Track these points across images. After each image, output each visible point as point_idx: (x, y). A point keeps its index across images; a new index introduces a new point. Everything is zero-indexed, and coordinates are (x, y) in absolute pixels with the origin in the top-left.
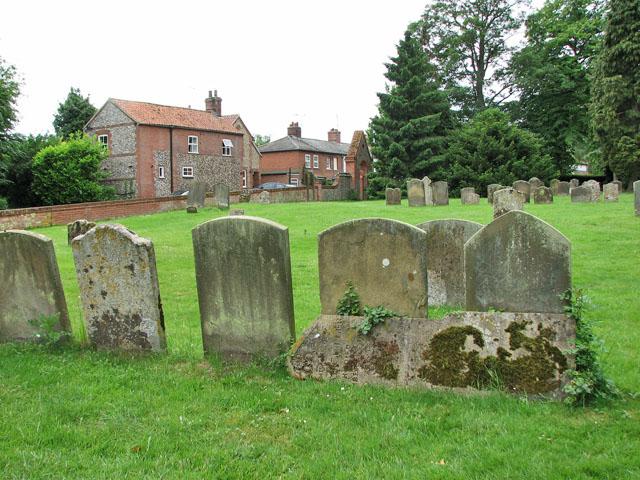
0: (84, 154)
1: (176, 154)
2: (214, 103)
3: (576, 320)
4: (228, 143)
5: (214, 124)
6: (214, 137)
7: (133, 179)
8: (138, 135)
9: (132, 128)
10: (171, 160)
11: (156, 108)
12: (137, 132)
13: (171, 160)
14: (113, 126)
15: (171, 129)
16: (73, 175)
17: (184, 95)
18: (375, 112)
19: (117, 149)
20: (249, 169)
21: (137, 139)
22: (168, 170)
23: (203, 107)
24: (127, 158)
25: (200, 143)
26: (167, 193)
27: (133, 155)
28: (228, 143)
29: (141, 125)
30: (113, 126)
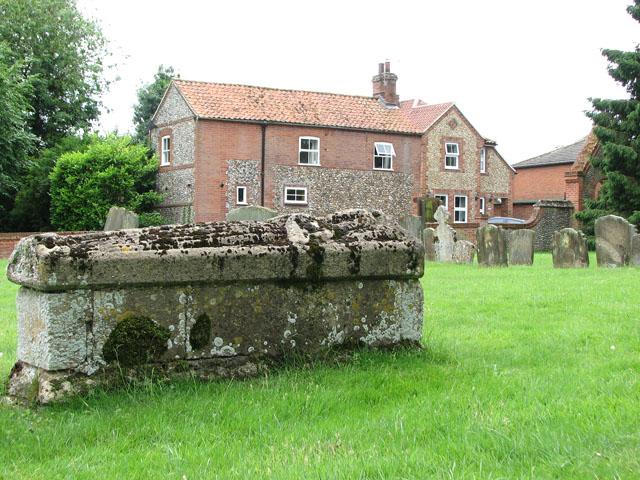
0: (107, 163)
1: (270, 165)
2: (386, 83)
3: (34, 290)
4: (386, 149)
5: (378, 117)
6: (354, 139)
7: (191, 204)
8: (198, 137)
9: (192, 125)
10: (263, 176)
11: (256, 94)
12: (197, 131)
13: (263, 176)
14: (176, 123)
15: (263, 126)
16: (89, 196)
17: (325, 69)
18: (397, 94)
19: (178, 161)
20: (473, 194)
21: (198, 143)
22: (256, 192)
23: (368, 90)
24: (185, 171)
25: (324, 149)
26: (392, 235)
27: (190, 166)
28: (386, 149)
29: (200, 119)
30: (176, 123)
